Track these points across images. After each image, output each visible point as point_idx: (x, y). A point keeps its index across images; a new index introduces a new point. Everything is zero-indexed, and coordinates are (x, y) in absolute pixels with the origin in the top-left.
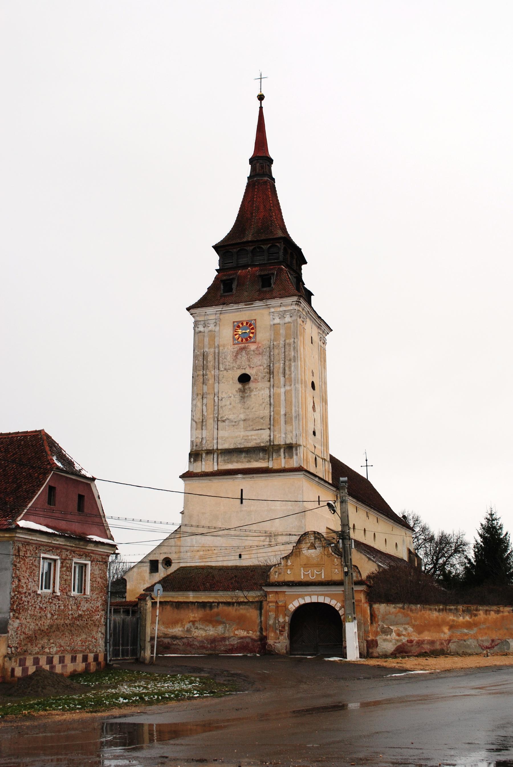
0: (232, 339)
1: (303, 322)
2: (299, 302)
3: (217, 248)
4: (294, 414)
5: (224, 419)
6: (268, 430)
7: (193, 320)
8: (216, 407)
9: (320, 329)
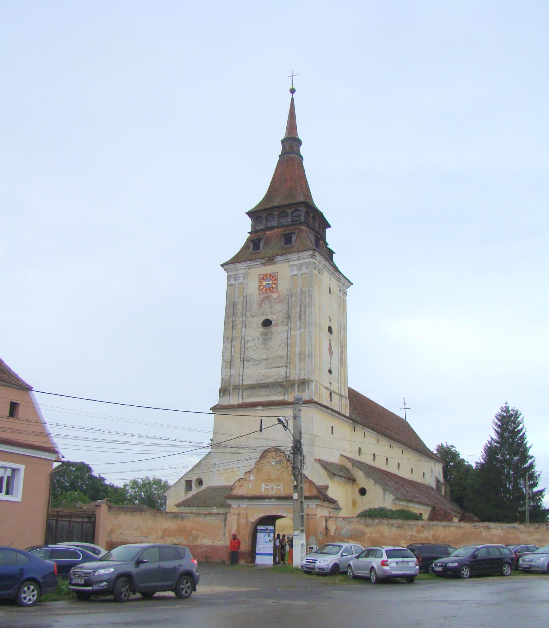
0: (257, 289)
3: (250, 214)
4: (307, 353)
6: (285, 368)
7: (226, 274)
8: (243, 349)
9: (340, 282)
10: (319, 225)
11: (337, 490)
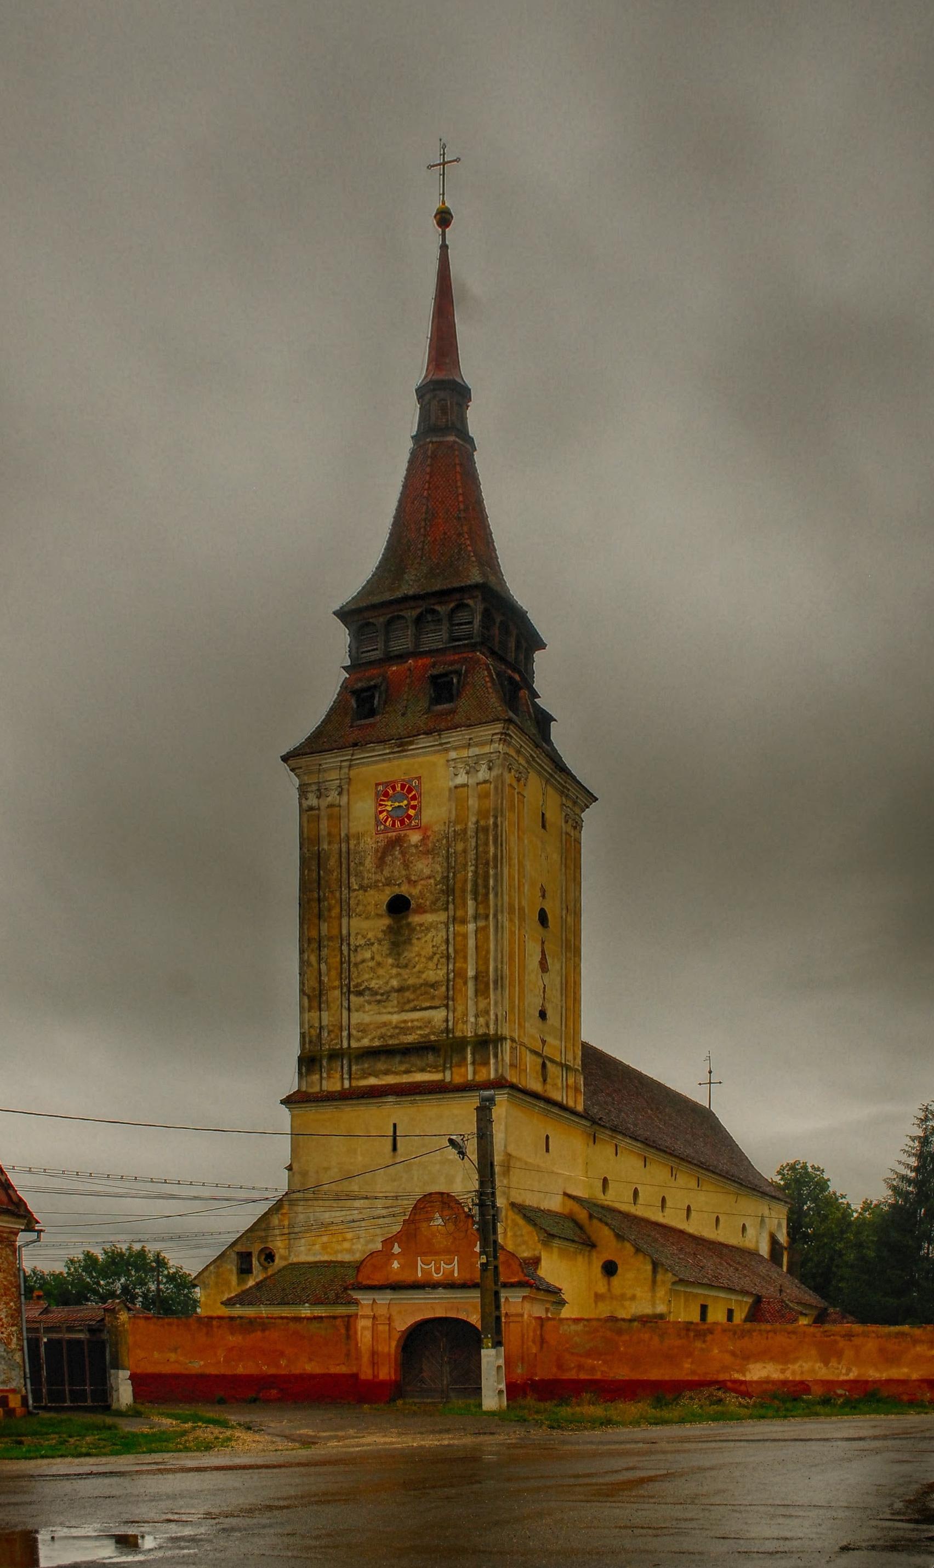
1: (519, 780)
2: (506, 734)
3: (344, 615)
5: (362, 988)
7: (297, 782)
10: (518, 647)
11: (555, 1268)
